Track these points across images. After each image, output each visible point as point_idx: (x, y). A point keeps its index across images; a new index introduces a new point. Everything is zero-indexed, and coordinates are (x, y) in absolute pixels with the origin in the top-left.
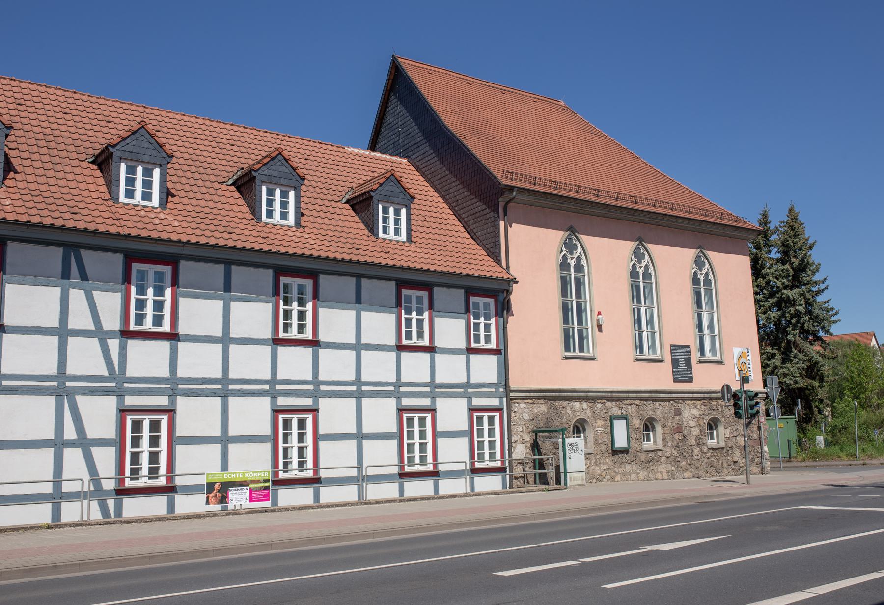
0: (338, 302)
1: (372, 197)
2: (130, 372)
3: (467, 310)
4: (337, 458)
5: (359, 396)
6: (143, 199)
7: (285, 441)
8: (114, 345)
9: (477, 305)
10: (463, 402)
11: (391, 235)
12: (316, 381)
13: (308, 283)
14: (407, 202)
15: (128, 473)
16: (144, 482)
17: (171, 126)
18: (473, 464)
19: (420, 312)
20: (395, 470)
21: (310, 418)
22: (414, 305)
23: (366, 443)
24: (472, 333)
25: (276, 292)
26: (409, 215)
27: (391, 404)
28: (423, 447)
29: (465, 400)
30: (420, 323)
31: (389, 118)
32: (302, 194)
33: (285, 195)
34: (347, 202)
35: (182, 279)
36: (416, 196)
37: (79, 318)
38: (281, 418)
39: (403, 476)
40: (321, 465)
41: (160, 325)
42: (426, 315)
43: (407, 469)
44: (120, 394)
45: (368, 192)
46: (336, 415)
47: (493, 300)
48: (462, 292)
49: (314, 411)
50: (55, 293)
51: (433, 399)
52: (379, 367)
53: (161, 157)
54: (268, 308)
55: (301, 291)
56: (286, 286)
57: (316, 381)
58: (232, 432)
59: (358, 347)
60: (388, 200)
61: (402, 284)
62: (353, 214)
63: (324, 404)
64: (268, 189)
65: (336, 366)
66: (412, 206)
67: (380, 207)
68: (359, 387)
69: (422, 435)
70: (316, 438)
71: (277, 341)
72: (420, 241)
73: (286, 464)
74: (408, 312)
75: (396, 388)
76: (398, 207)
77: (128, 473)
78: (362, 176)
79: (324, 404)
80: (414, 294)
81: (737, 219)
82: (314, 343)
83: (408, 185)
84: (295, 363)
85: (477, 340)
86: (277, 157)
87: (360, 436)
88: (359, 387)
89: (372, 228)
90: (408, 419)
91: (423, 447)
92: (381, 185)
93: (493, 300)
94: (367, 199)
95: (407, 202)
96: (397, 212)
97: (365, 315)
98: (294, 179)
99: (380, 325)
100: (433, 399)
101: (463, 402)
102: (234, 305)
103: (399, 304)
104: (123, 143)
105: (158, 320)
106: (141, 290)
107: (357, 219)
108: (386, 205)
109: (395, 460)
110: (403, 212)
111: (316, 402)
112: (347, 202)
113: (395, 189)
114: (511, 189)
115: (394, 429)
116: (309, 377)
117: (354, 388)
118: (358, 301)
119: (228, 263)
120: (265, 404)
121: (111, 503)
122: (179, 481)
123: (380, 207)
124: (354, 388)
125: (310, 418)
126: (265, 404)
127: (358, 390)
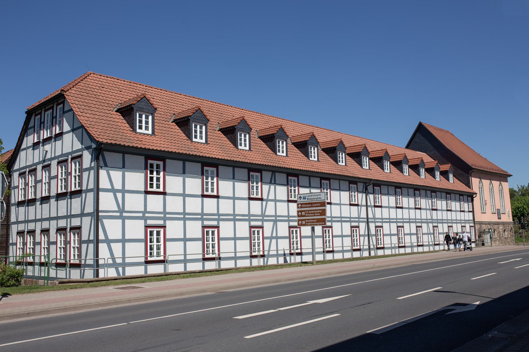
0: (175, 173)
1: (189, 120)
2: (126, 209)
3: (249, 180)
4: (227, 248)
5: (184, 220)
6: (146, 130)
7: (151, 242)
8: (119, 195)
9: (207, 171)
10: (247, 223)
11: (143, 131)
12: (165, 212)
13: (161, 163)
14: (249, 131)
15: (149, 255)
16: (155, 258)
17: (156, 97)
18: (146, 258)
19: (295, 187)
20: (201, 257)
21: (162, 230)
22: (325, 187)
23: (188, 243)
24: (205, 187)
25: (146, 168)
26: (206, 129)
27: (199, 224)
28: (158, 248)
29: (201, 222)
30: (212, 183)
31: (415, 140)
32: (155, 118)
33: (147, 117)
34: (220, 130)
35: (167, 169)
36: (211, 120)
37: (104, 183)
38: (149, 230)
39: (147, 262)
40: (221, 251)
41: (159, 188)
42: (260, 184)
43: (149, 259)
44: (145, 219)
45: (188, 116)
46: (174, 229)
47: (162, 162)
48: (143, 157)
49: (164, 227)
50: (181, 179)
51: (165, 221)
52: (194, 205)
53: (152, 110)
54: (142, 175)
55: (158, 166)
56: (207, 171)
57: (165, 212)
58: (127, 238)
59: (184, 195)
60: (142, 110)
61: (322, 179)
62: (122, 118)
63: (222, 224)
64: (139, 114)
65: (174, 205)
66: (156, 115)
67: (138, 114)
68: (202, 216)
69: (158, 241)
70: (263, 238)
71: (147, 192)
72: (211, 143)
73: (151, 253)
74: (253, 183)
75: (202, 216)
76: (201, 125)
77: (149, 255)
78: (128, 97)
79: (168, 223)
80: (210, 169)
81: (504, 171)
82: (164, 193)
83: (250, 124)
84: (155, 203)
85: (207, 191)
86: (144, 98)
87: (185, 240)
88: (202, 216)
89: (132, 125)
90: (207, 232)
91: (158, 248)
92: (194, 113)
93: (162, 162)
94: (186, 120)
95: (249, 131)
96: (201, 128)
97: (187, 179)
98: (152, 110)
99: (194, 184)
100: (165, 221)
101: (247, 223)
102: (187, 179)
103: (249, 180)
104: (137, 104)
105: (158, 187)
106: (207, 179)
107: (124, 121)
108: (141, 113)
109: (143, 254)
110: (204, 127)
111: (218, 223)
112: (220, 130)
113: (200, 115)
114: (474, 169)
115: (143, 237)
116: (162, 210)
117: (162, 215)
118: (234, 178)
119: (234, 167)
120: (142, 223)
121: (120, 269)
122: (222, 255)
123: (138, 114)
124: (162, 215)
125: (162, 230)
126: (142, 223)
127: (185, 217)
